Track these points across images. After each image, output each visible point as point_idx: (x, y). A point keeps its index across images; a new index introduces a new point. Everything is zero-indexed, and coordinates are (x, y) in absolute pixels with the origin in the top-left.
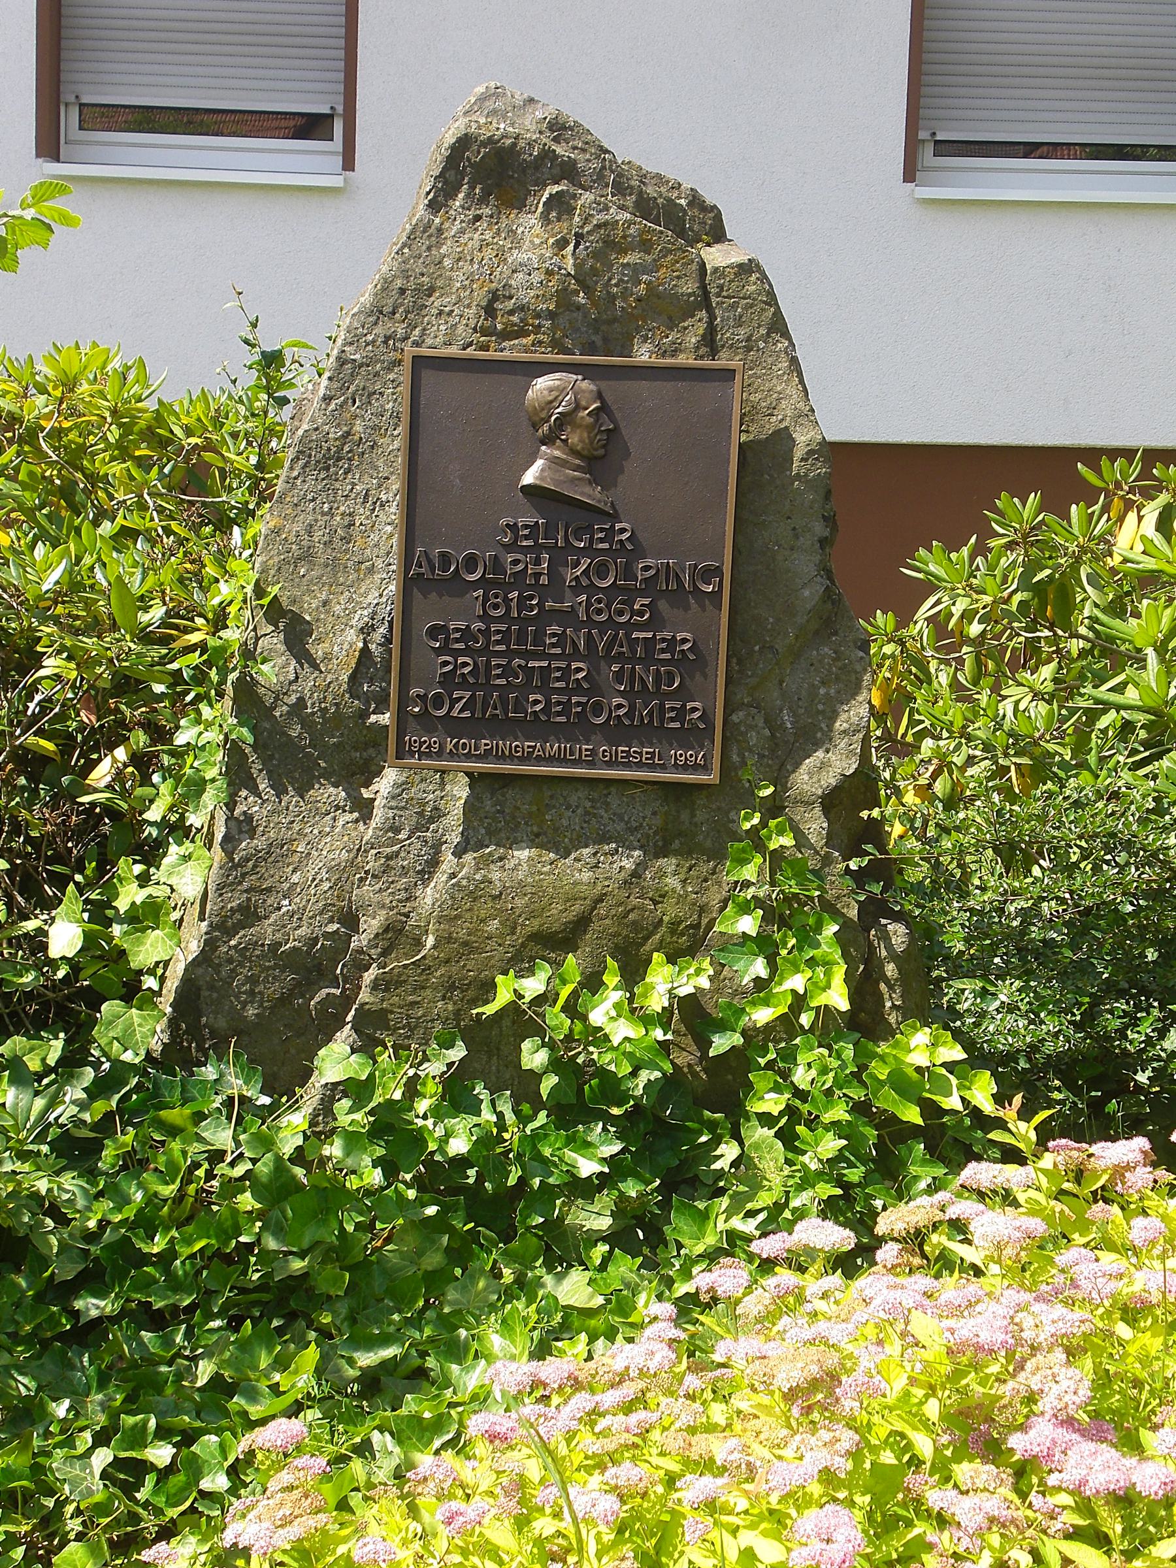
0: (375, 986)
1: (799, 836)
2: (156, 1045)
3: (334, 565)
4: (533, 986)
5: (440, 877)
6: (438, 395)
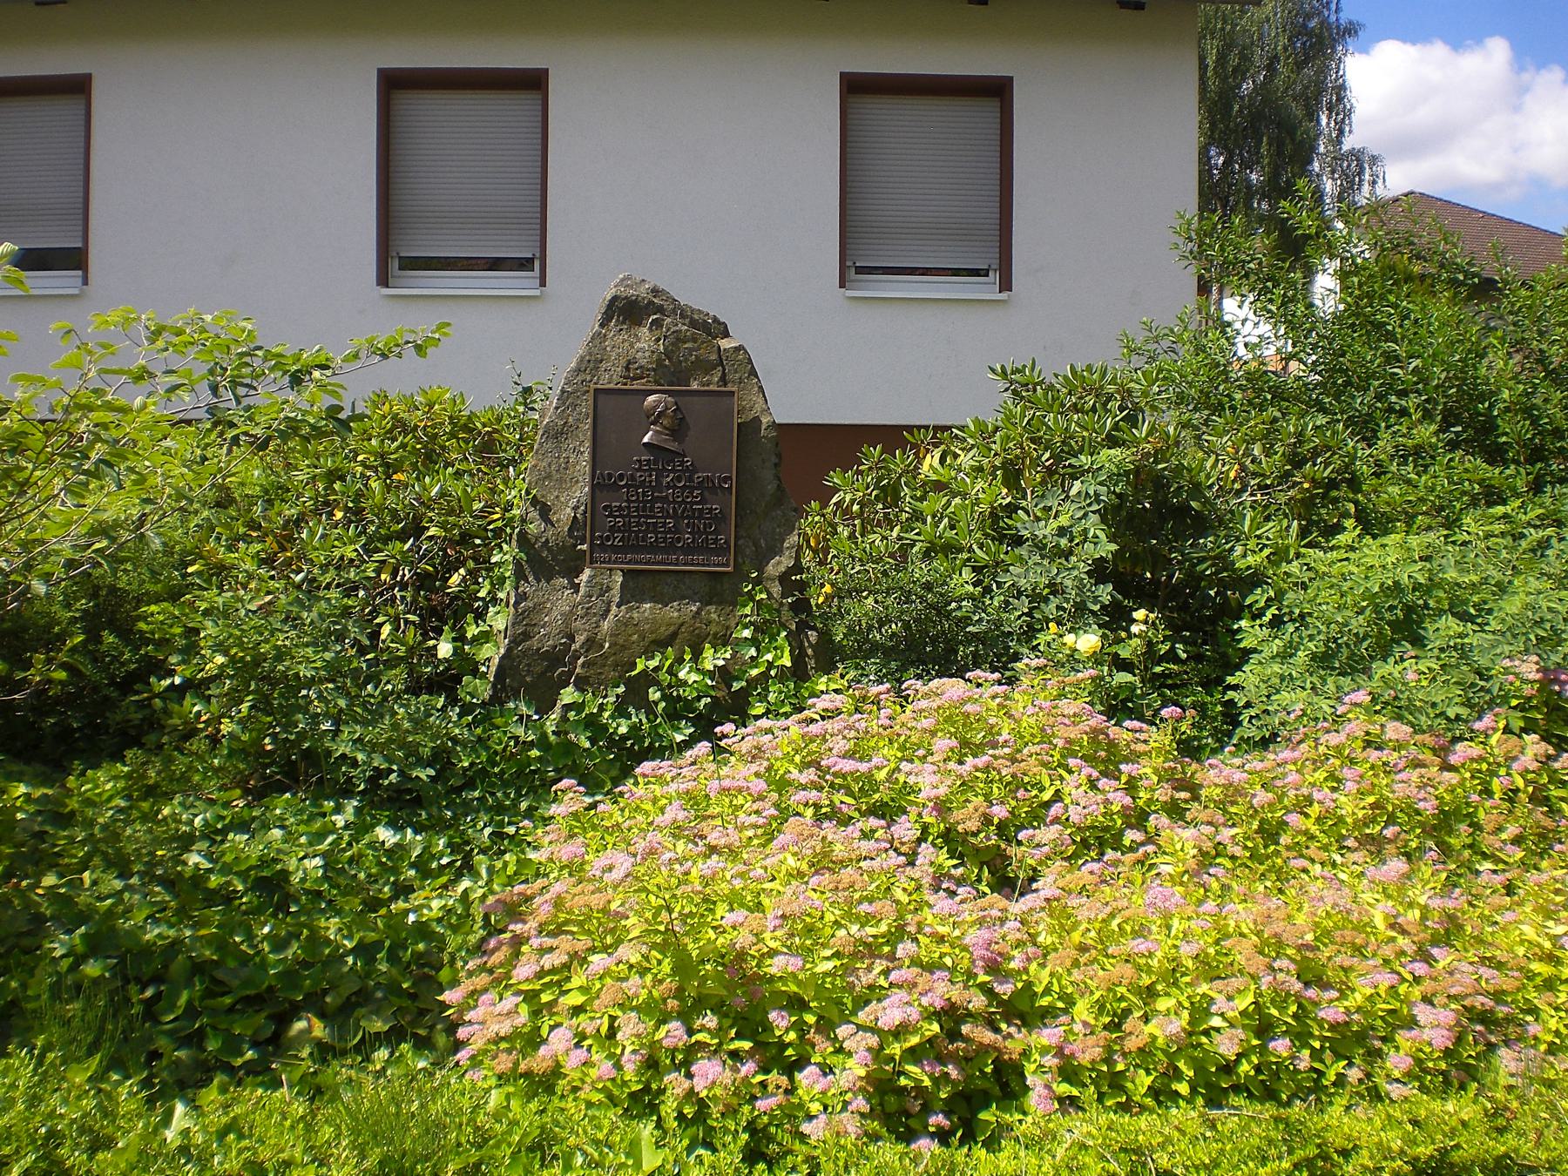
0: (583, 666)
1: (769, 594)
2: (486, 696)
3: (561, 480)
4: (653, 664)
5: (611, 616)
6: (604, 405)
